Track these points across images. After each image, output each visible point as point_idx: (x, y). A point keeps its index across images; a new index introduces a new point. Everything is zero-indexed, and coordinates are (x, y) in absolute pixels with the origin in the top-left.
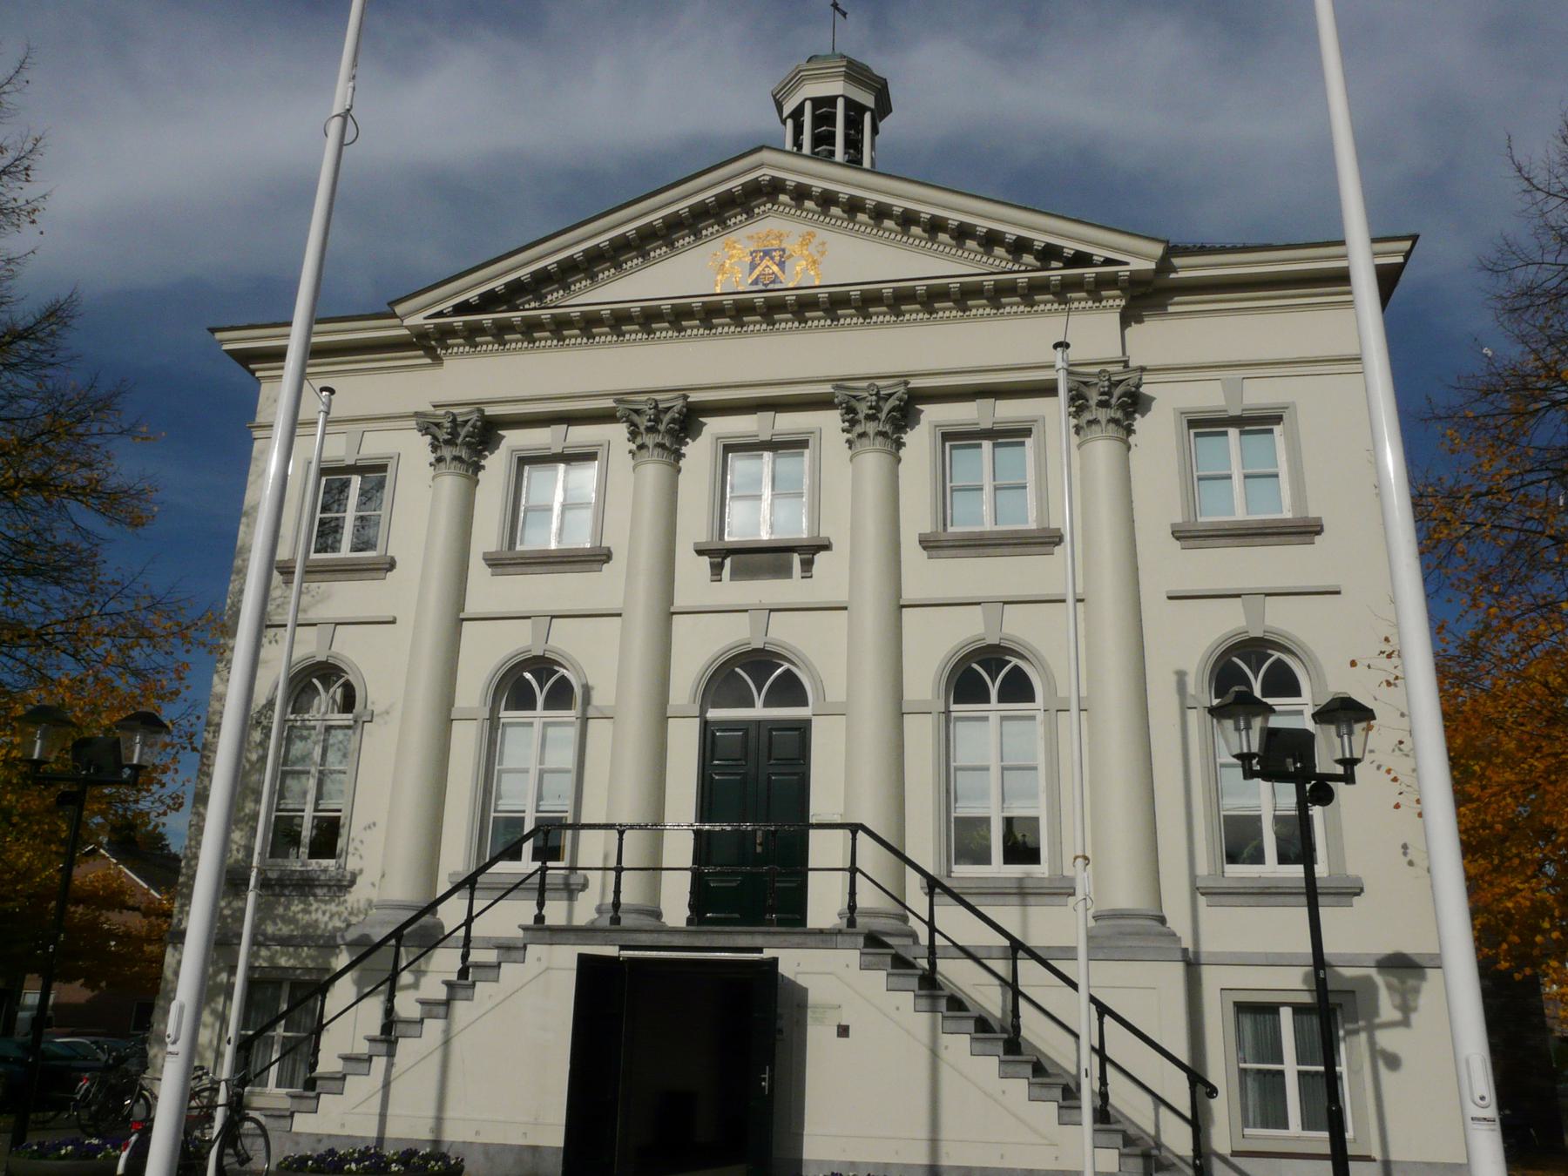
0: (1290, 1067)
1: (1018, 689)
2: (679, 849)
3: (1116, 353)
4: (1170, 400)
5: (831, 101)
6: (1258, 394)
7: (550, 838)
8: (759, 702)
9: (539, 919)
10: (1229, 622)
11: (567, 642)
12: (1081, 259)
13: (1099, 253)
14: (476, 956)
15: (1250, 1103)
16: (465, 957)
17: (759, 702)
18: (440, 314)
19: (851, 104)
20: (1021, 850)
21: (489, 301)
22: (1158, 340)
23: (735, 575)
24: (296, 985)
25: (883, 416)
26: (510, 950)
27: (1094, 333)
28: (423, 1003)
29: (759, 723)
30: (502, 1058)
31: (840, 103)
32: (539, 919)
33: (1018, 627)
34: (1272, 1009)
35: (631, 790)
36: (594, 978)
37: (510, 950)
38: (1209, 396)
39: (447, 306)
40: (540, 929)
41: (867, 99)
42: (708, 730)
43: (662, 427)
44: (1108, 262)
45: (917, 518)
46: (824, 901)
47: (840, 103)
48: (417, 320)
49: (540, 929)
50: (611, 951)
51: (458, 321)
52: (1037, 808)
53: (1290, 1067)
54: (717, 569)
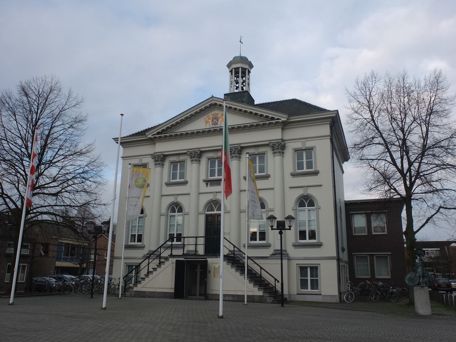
0: (309, 278)
1: (311, 204)
2: (201, 241)
3: (280, 137)
4: (291, 147)
5: (238, 68)
6: (309, 144)
7: (179, 237)
8: (215, 210)
9: (171, 254)
10: (301, 192)
11: (181, 200)
12: (273, 119)
13: (276, 117)
14: (161, 260)
15: (149, 289)
16: (160, 260)
17: (215, 210)
18: (154, 135)
19: (242, 68)
20: (313, 235)
21: (158, 133)
22: (291, 134)
23: (211, 185)
24: (312, 268)
25: (236, 152)
26: (167, 259)
27: (275, 134)
28: (153, 268)
29: (215, 214)
30: (163, 279)
31: (240, 69)
32: (171, 254)
33: (311, 192)
34: (306, 268)
35: (193, 227)
36: (179, 265)
37: (167, 259)
38: (299, 145)
39: (155, 133)
40: (172, 256)
41: (246, 66)
42: (207, 216)
43: (196, 156)
44: (278, 119)
45: (203, 176)
46: (223, 251)
47: (240, 69)
48: (150, 136)
49: (172, 256)
50: (183, 259)
51: (157, 136)
52: (313, 228)
53: (309, 278)
54: (207, 184)
